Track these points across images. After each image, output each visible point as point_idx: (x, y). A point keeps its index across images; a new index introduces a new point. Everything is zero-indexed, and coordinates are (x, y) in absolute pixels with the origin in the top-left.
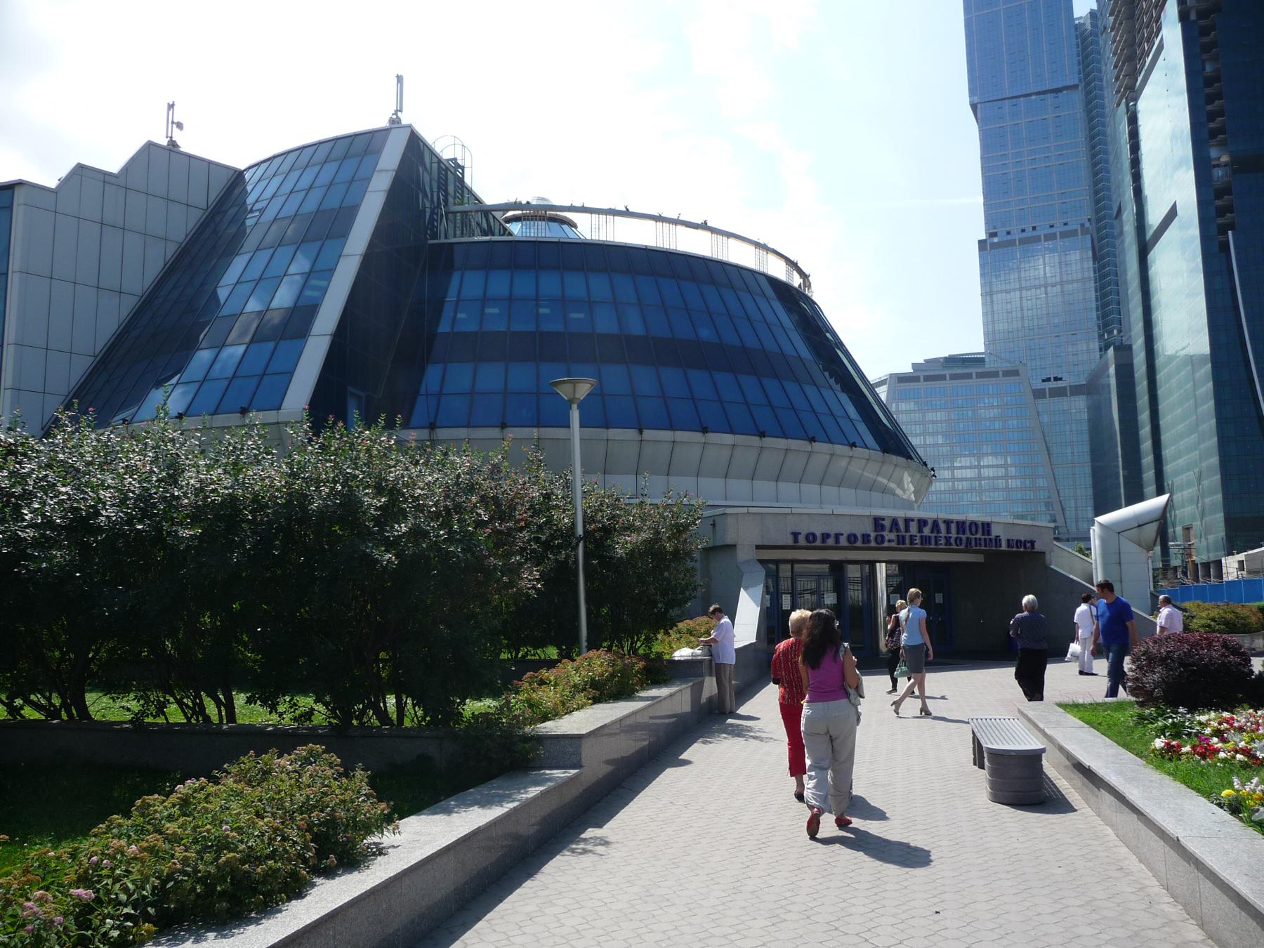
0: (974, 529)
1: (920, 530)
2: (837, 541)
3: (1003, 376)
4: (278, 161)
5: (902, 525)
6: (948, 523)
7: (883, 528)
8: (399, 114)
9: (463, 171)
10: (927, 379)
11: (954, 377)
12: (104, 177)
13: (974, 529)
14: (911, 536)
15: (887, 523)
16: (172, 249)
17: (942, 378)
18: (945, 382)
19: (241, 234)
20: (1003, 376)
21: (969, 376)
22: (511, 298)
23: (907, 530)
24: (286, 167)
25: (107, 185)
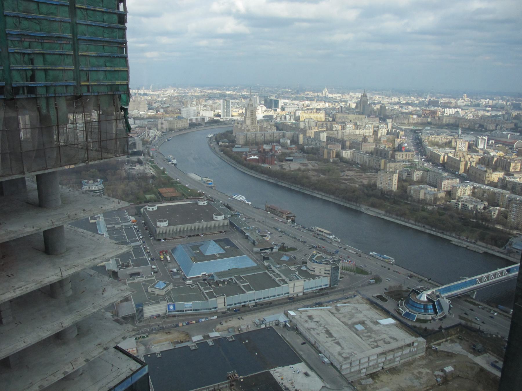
25: (39, 4)
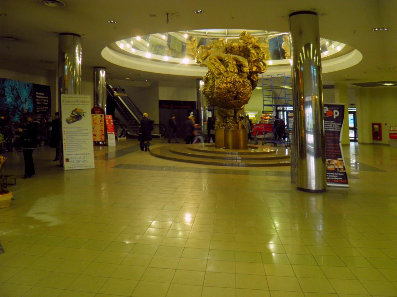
25: (182, 257)
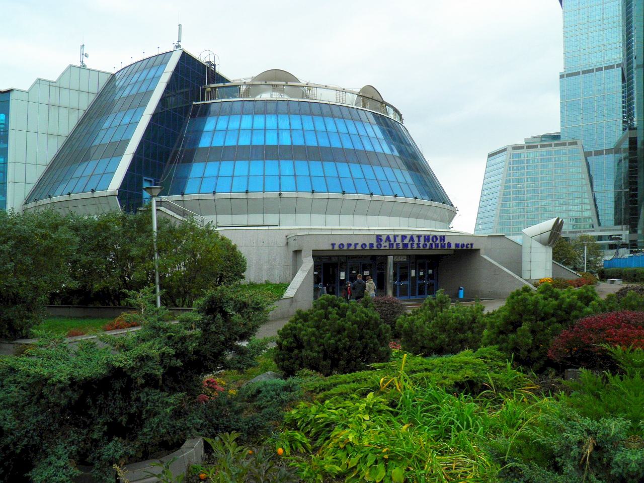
0: (435, 240)
1: (402, 241)
2: (355, 247)
3: (540, 147)
4: (126, 69)
5: (392, 238)
6: (419, 237)
7: (381, 240)
8: (179, 43)
9: (215, 67)
10: (528, 147)
11: (542, 146)
12: (50, 84)
13: (435, 240)
14: (397, 244)
15: (384, 238)
16: (81, 114)
17: (536, 147)
18: (566, 147)
19: (112, 104)
20: (540, 147)
21: (550, 145)
22: (227, 130)
23: (395, 241)
24: (135, 70)
25: (205, 176)
